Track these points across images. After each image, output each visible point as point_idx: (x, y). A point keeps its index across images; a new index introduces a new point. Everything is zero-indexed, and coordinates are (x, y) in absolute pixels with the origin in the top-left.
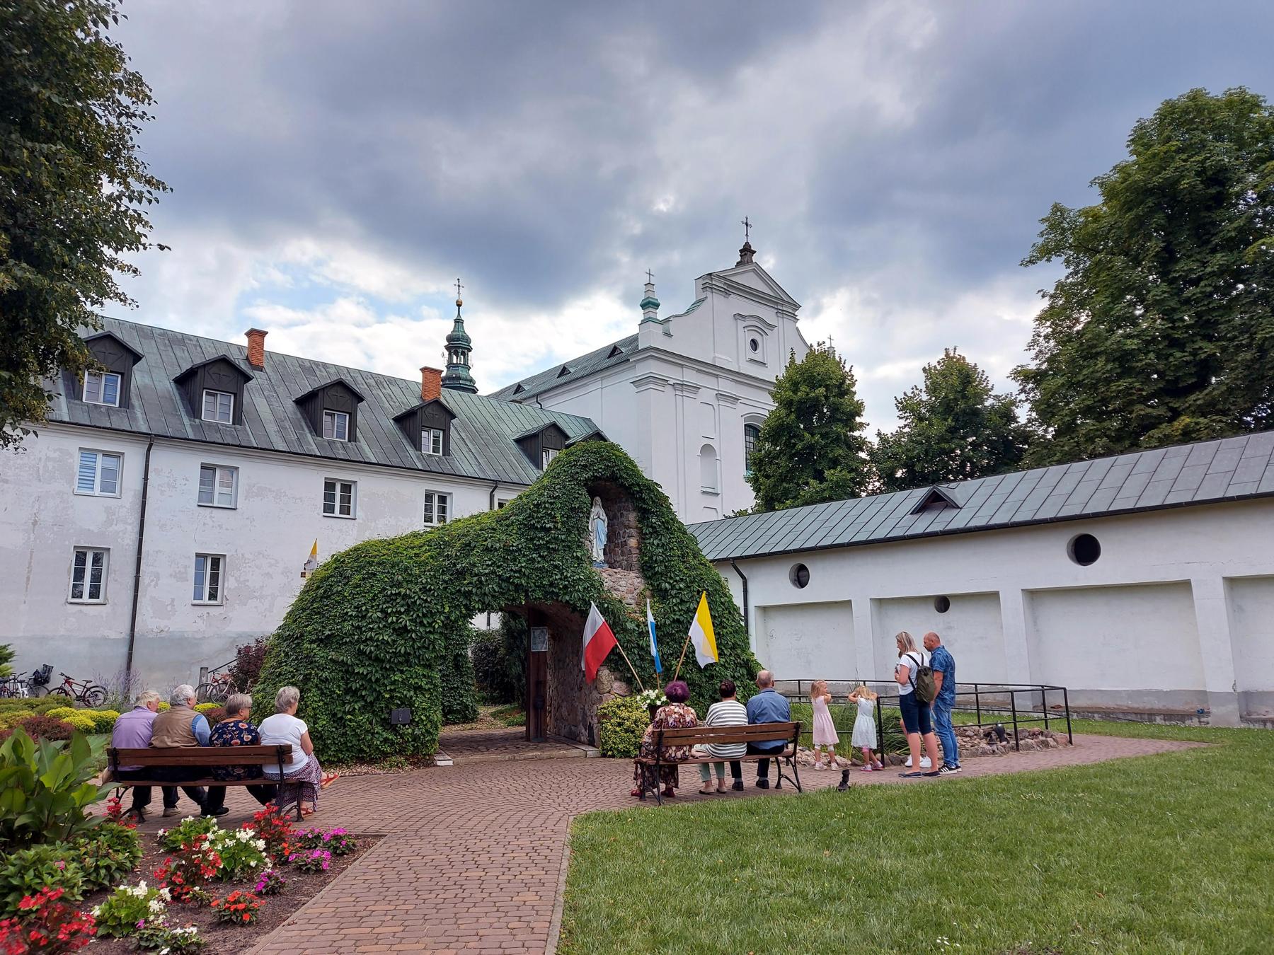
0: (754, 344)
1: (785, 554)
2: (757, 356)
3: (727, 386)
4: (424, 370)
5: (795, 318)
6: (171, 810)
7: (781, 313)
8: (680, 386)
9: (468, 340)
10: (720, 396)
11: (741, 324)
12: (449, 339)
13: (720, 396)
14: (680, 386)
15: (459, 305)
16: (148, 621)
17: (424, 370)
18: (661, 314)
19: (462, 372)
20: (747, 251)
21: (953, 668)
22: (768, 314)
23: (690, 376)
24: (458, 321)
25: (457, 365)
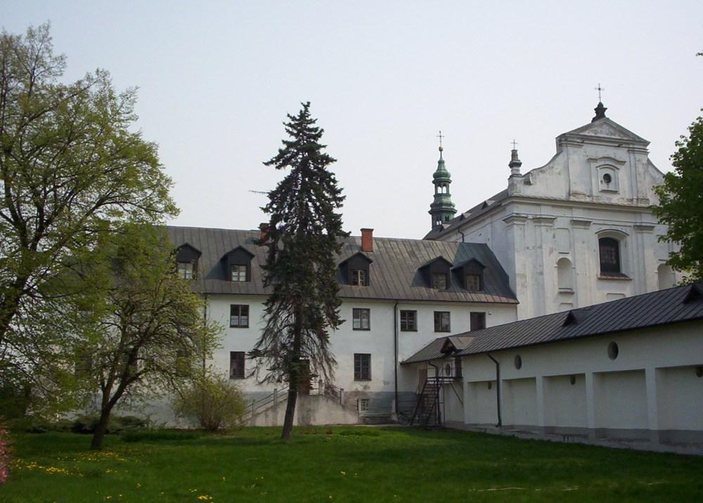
0: (607, 178)
1: (512, 348)
2: (611, 187)
3: (579, 214)
4: (362, 230)
5: (646, 153)
6: (22, 276)
7: (631, 151)
8: (538, 220)
9: (447, 175)
10: (575, 222)
11: (594, 165)
12: (435, 176)
13: (575, 222)
14: (538, 220)
15: (441, 150)
16: (398, 390)
17: (362, 230)
18: (523, 170)
19: (445, 200)
20: (600, 110)
21: (604, 430)
22: (621, 154)
23: (546, 211)
24: (441, 163)
25: (442, 195)
